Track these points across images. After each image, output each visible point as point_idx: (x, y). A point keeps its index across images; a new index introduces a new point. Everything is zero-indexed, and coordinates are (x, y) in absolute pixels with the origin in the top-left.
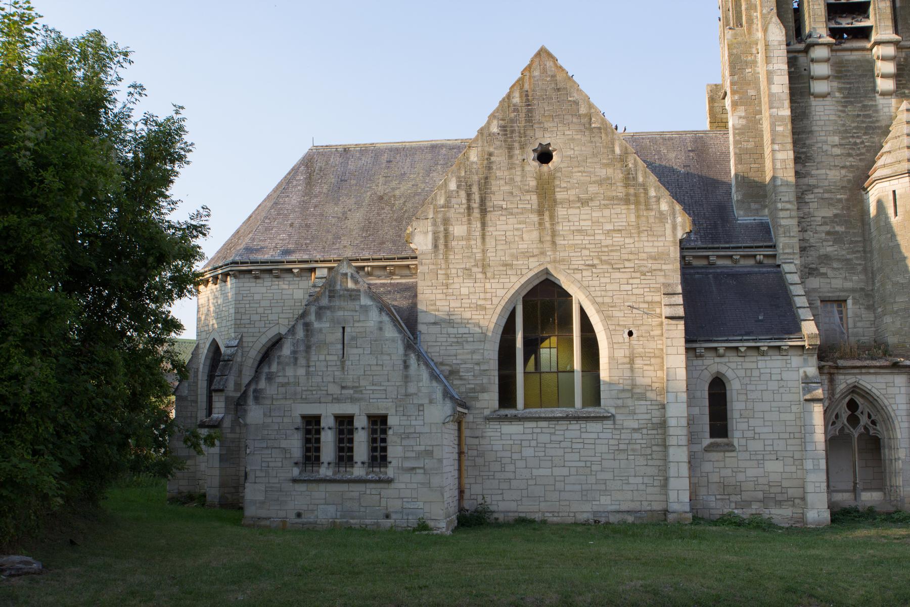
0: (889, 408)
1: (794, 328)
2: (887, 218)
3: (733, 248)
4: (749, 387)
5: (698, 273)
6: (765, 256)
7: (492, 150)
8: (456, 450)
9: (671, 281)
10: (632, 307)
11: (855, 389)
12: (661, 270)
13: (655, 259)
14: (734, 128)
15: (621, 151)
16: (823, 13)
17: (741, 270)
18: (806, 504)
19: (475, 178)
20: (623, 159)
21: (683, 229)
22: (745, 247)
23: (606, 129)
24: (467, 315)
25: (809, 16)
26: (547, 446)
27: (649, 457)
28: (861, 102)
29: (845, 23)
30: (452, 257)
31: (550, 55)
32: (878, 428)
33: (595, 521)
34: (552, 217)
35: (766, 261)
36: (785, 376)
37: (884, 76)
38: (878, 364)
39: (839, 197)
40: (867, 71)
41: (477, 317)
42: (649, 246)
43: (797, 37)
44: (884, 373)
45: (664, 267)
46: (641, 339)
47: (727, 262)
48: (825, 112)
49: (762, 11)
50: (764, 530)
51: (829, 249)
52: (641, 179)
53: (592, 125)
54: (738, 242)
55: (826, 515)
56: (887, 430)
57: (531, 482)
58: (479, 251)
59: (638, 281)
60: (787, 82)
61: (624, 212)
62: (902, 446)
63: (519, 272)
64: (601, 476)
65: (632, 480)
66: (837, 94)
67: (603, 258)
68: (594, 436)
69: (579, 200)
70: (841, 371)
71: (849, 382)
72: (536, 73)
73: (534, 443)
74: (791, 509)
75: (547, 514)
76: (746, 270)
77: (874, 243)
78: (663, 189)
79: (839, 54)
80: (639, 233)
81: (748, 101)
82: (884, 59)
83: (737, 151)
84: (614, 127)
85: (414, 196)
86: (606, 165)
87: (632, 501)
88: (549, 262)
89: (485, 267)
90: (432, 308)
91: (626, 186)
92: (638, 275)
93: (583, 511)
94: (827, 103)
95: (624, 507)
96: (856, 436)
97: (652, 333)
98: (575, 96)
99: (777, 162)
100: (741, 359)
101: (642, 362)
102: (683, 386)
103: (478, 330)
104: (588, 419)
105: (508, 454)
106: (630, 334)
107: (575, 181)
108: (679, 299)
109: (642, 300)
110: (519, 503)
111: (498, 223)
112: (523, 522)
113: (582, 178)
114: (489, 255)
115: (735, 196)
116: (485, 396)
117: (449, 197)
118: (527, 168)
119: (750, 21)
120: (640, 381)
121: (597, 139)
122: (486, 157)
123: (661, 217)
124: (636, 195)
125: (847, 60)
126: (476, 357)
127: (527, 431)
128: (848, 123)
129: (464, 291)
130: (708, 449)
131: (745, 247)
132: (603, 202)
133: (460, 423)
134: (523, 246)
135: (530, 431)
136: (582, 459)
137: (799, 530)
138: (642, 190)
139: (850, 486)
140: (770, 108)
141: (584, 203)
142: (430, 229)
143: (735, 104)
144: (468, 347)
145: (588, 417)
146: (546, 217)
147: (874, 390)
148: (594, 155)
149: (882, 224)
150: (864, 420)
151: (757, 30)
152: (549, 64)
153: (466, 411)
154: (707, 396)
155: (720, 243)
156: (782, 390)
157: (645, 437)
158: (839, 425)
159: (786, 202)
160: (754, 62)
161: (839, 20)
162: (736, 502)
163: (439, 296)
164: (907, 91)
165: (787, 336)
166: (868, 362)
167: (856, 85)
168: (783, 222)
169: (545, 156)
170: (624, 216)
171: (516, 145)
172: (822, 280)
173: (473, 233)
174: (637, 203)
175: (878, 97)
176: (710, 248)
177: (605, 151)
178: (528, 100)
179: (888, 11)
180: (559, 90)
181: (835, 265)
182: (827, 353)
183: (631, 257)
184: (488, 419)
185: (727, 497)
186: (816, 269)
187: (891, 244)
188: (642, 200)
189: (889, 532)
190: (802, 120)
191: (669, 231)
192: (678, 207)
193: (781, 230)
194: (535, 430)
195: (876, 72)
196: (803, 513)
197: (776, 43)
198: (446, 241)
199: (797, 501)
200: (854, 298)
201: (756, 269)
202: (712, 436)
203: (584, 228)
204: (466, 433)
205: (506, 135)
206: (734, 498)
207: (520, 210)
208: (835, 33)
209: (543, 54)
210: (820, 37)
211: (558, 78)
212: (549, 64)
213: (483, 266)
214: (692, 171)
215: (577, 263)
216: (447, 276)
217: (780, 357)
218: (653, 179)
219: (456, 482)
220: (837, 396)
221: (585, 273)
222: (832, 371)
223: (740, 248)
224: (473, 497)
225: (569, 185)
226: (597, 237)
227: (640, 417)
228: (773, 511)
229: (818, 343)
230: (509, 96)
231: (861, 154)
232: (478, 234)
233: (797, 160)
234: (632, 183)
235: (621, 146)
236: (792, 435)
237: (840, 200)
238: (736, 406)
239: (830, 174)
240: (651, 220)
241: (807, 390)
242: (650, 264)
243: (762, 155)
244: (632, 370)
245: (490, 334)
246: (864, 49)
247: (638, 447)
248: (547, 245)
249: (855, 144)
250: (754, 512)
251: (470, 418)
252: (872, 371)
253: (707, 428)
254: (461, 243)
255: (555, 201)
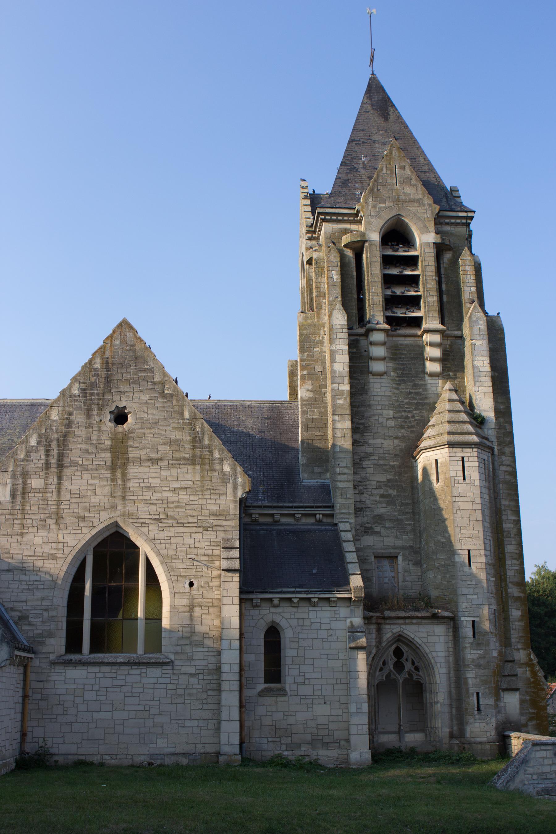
0: (430, 656)
1: (343, 581)
2: (431, 483)
3: (295, 507)
4: (301, 636)
5: (263, 529)
6: (323, 515)
7: (72, 410)
8: (21, 693)
9: (230, 536)
10: (194, 560)
11: (400, 638)
12: (221, 526)
13: (217, 516)
14: (302, 400)
15: (190, 416)
16: (381, 303)
17: (302, 527)
18: (350, 746)
19: (55, 435)
20: (191, 423)
21: (243, 488)
22: (306, 507)
23: (179, 397)
24: (39, 563)
25: (369, 306)
26: (109, 690)
27: (204, 701)
28: (413, 381)
29: (400, 313)
30: (28, 508)
31: (130, 327)
32: (421, 673)
33: (149, 764)
34: (124, 474)
35: (325, 520)
36: (333, 625)
37: (432, 360)
38: (420, 615)
39: (392, 464)
40: (418, 354)
41: (49, 565)
42: (212, 504)
43: (359, 322)
44: (425, 624)
45: (224, 523)
46: (201, 589)
47: (291, 520)
48: (381, 389)
49: (329, 298)
50: (308, 771)
51: (383, 510)
52: (206, 442)
53: (166, 391)
54: (301, 502)
55: (367, 756)
56: (429, 675)
57: (92, 725)
58: (54, 503)
59: (200, 535)
60: (348, 361)
61: (189, 471)
62: (441, 690)
63: (90, 525)
64: (158, 719)
65: (188, 723)
66: (392, 374)
67: (169, 513)
68: (153, 680)
69: (150, 459)
70: (388, 621)
71: (394, 631)
72: (117, 343)
73: (96, 687)
74: (337, 750)
75: (107, 757)
76: (306, 527)
77: (421, 505)
78: (226, 452)
79: (395, 339)
80: (203, 491)
81: (317, 378)
82: (432, 345)
83: (304, 420)
84: (185, 394)
85: (8, 450)
86: (176, 428)
87: (187, 743)
88: (119, 516)
89: (58, 518)
90: (6, 555)
91: (193, 448)
92: (200, 530)
93: (141, 753)
94: (383, 381)
95: (179, 750)
96: (401, 681)
97: (211, 584)
98: (152, 365)
99: (339, 430)
100: (295, 610)
101: (201, 611)
102: (236, 634)
103: (48, 578)
104: (148, 664)
105: (71, 698)
106: (191, 584)
107: (147, 442)
108: (236, 553)
109: (203, 553)
110: (79, 746)
111: (73, 477)
112: (82, 765)
113: (153, 439)
114: (63, 507)
115: (302, 460)
116: (52, 641)
117: (29, 452)
118: (104, 428)
119: (319, 307)
120: (199, 629)
121: (169, 404)
122: (66, 416)
123: (224, 478)
124: (201, 457)
125: (401, 345)
126: (46, 603)
127: (90, 675)
128: (401, 399)
129: (38, 540)
130: (262, 694)
131: (306, 507)
132: (171, 462)
133: (25, 667)
134: (95, 500)
135: (93, 675)
136: (141, 702)
137: (344, 771)
138: (207, 452)
139: (395, 728)
140: (332, 383)
141: (154, 462)
142: (9, 481)
143: (303, 378)
144: (39, 594)
145: (148, 663)
146: (119, 475)
147: (417, 639)
148: (166, 419)
149: (427, 489)
150: (408, 666)
151: (325, 315)
152: (130, 335)
153: (32, 656)
154: (263, 644)
155: (285, 502)
156: (330, 639)
157: (201, 682)
158: (386, 672)
159: (344, 467)
160: (322, 342)
161: (395, 310)
162: (286, 744)
163: (13, 545)
164: (451, 374)
165: (335, 589)
166: (411, 613)
167: (409, 367)
168: (341, 485)
169: (120, 418)
170: (190, 475)
171: (95, 407)
172: (376, 538)
173: (50, 487)
174: (202, 464)
175: (427, 377)
176: (275, 507)
177: (176, 415)
178: (108, 366)
179: (436, 304)
180: (136, 358)
181: (388, 525)
182: (374, 605)
183: (195, 513)
184: (54, 663)
185: (278, 739)
186: (371, 528)
187: (433, 507)
188: (207, 461)
189: (419, 771)
190: (361, 395)
191: (230, 491)
192: (239, 469)
193: (338, 492)
194: (98, 675)
195: (426, 356)
196: (347, 755)
197: (339, 327)
198: (24, 493)
199: (343, 743)
200: (403, 555)
201: (316, 527)
202: (266, 681)
203: (152, 485)
204: (31, 676)
205: (86, 397)
206: (285, 740)
207: (94, 467)
208: (389, 320)
209: (125, 325)
210: (378, 324)
211: (137, 347)
212: (130, 335)
213: (58, 518)
214: (266, 437)
215: (145, 517)
216: (23, 526)
217: (329, 608)
218: (217, 442)
219: (19, 725)
220: (384, 644)
221: (151, 527)
222: (379, 621)
223: (302, 507)
224: (34, 740)
225: (141, 446)
226: (165, 494)
227: (198, 663)
228: (321, 752)
229: (363, 595)
230: (91, 362)
231: (412, 427)
232: (54, 487)
233: (355, 430)
234: (198, 445)
235: (190, 411)
236: (339, 681)
237: (393, 467)
238: (289, 653)
239: (384, 443)
240: (215, 480)
241: (353, 639)
242: (211, 520)
243: (326, 424)
244: (191, 618)
245: (60, 582)
246: (415, 336)
247: (195, 691)
248: (118, 500)
249: (407, 417)
250: (303, 753)
251: (36, 662)
252: (415, 621)
253: (262, 674)
254: (37, 495)
255: (127, 459)
